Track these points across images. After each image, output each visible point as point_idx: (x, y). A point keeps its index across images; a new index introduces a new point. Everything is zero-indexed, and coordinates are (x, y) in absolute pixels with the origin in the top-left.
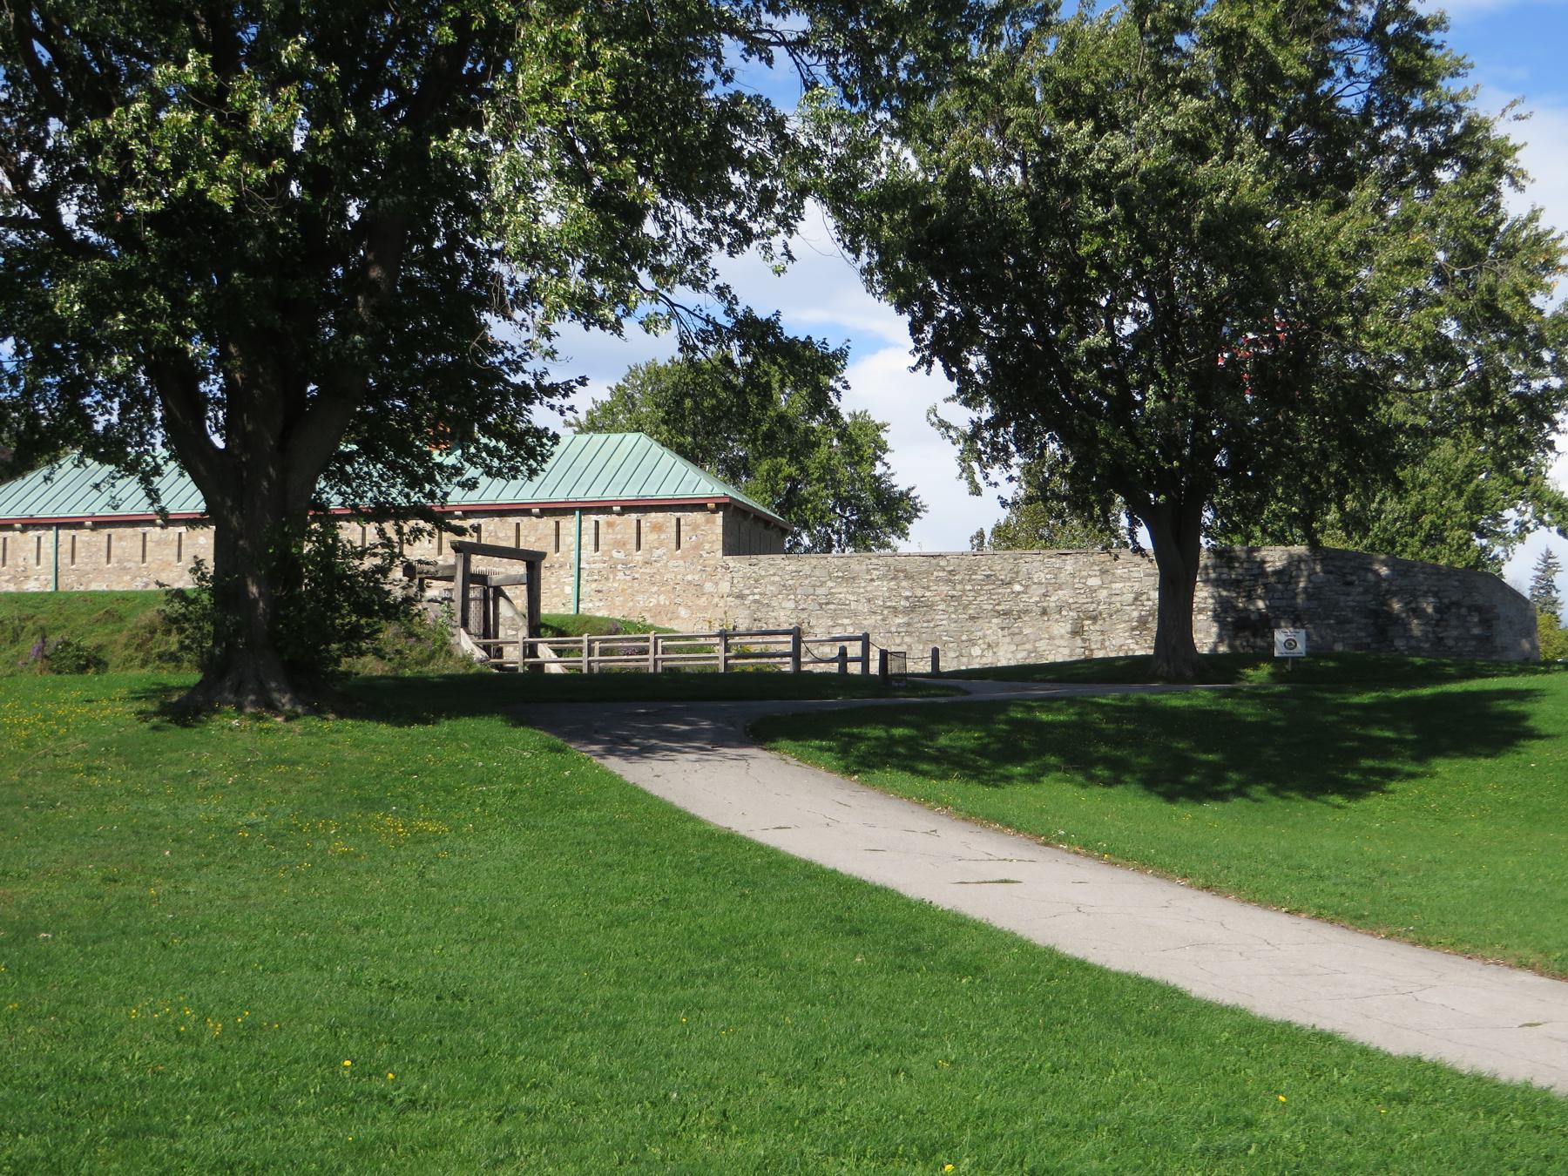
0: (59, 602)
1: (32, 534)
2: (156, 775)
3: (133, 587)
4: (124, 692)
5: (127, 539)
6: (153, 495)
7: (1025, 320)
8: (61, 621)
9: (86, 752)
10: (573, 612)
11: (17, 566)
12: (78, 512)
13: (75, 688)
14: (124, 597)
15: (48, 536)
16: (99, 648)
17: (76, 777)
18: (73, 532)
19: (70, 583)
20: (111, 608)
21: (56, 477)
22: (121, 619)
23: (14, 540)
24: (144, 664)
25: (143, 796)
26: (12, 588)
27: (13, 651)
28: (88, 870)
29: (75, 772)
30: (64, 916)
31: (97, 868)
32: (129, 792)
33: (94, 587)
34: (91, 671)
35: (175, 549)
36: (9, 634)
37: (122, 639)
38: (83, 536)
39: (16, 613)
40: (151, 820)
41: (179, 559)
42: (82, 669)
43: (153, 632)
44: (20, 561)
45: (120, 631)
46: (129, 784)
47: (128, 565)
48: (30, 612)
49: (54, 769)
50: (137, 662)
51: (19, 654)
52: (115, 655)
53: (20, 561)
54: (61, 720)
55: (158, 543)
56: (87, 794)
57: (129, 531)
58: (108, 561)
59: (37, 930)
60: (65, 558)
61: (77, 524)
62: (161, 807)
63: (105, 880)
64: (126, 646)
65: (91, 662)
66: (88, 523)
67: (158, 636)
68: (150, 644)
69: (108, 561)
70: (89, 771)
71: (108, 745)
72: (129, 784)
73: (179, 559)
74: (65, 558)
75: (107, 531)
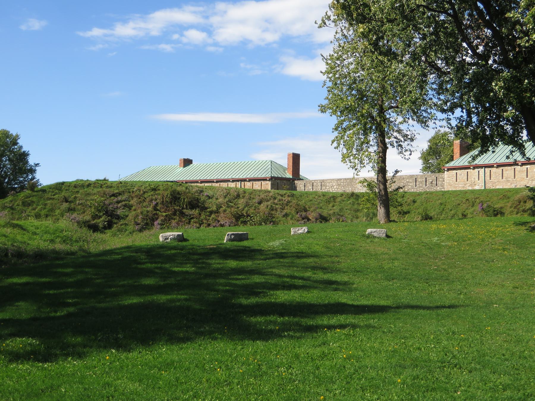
0: (487, 192)
1: (476, 170)
2: (528, 251)
3: (511, 187)
4: (513, 222)
5: (508, 171)
6: (523, 154)
7: (520, 76)
8: (488, 199)
9: (502, 243)
10: (483, 188)
11: (472, 181)
12: (492, 162)
13: (496, 221)
14: (509, 190)
15: (482, 171)
16: (501, 208)
17: (500, 252)
18: (490, 169)
19: (489, 186)
20: (505, 194)
21: (497, 151)
22: (508, 198)
23: (471, 172)
24: (517, 213)
25: (524, 259)
26: (470, 188)
27: (472, 209)
28: (507, 283)
29: (499, 250)
30: (501, 299)
31: (510, 283)
32: (519, 257)
33: (498, 187)
34: (499, 216)
35: (526, 173)
36: (471, 203)
37: (509, 205)
38: (494, 170)
39: (473, 197)
40: (528, 267)
41: (527, 177)
42: (496, 215)
43: (520, 202)
44: (473, 180)
45: (508, 202)
46: (518, 254)
47: (509, 179)
48: (477, 196)
49: (492, 249)
50: (515, 213)
51: (474, 211)
52: (507, 210)
53: (473, 180)
54: (492, 232)
55: (519, 172)
56: (504, 258)
57: (509, 168)
58: (502, 178)
59: (493, 304)
60: (488, 178)
61: (491, 166)
62: (530, 263)
63: (514, 288)
64: (511, 207)
65: (498, 213)
66: (495, 166)
67: (522, 203)
68: (519, 206)
69: (502, 178)
70: (504, 250)
71: (510, 241)
72: (518, 254)
73: (527, 177)
74: (488, 178)
75: (502, 168)
